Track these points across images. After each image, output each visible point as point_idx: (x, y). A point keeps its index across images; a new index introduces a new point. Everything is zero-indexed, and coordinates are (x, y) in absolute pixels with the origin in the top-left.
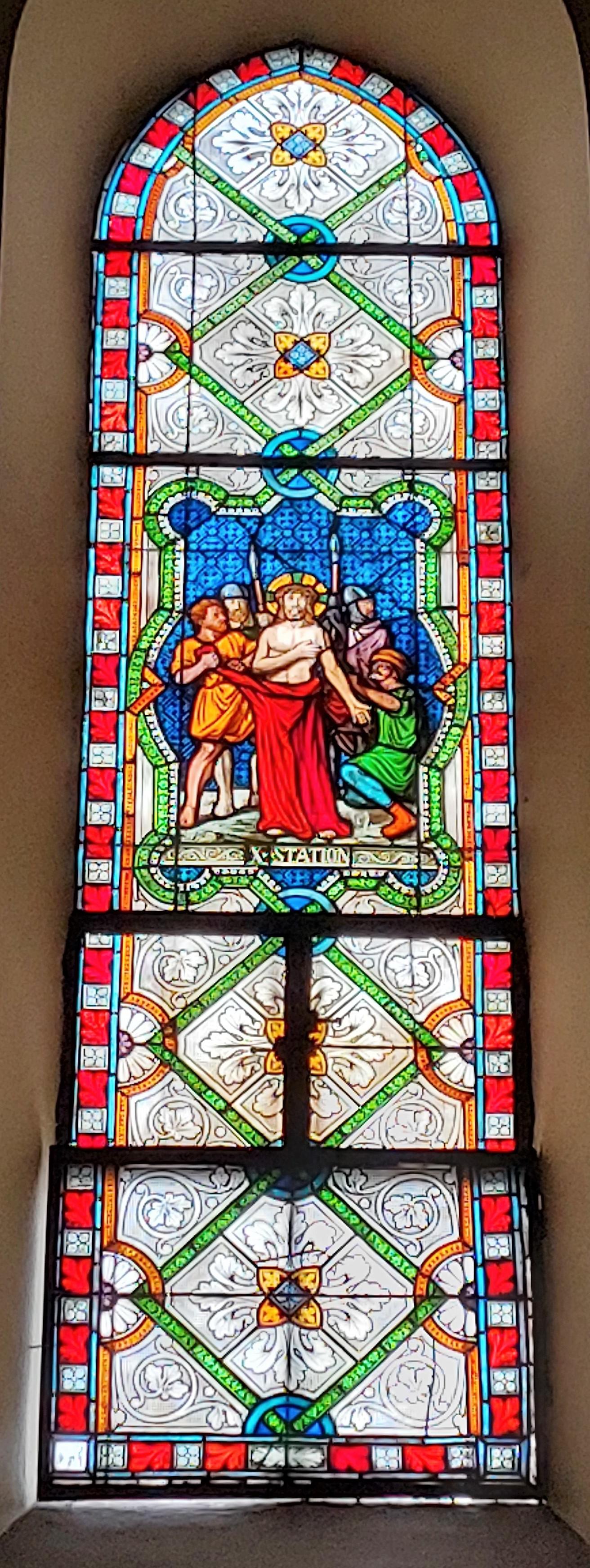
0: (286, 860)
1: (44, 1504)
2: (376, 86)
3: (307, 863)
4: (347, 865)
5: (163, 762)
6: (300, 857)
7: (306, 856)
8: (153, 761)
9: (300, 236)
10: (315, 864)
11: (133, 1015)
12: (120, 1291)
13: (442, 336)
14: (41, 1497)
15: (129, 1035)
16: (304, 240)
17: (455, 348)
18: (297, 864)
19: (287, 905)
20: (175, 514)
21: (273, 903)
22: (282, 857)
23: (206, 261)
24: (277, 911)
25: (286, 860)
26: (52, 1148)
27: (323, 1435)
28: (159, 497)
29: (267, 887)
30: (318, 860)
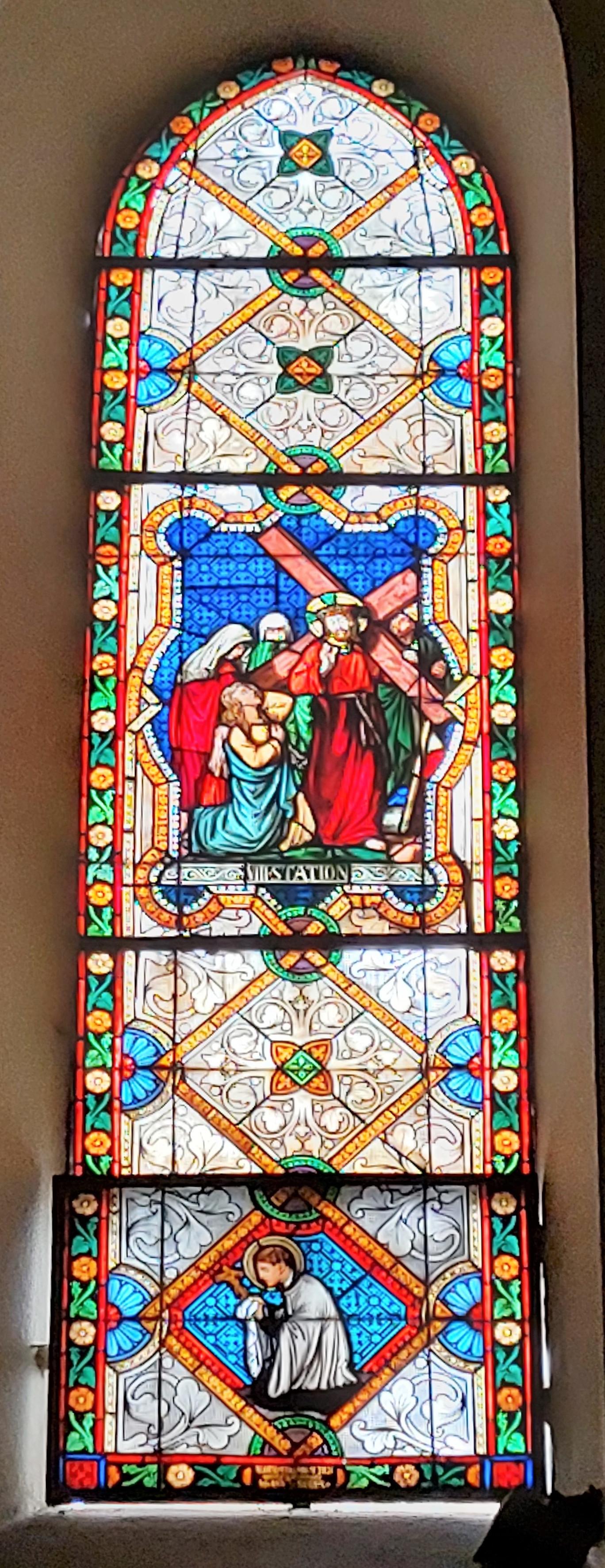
0: (283, 878)
1: (54, 1510)
2: (382, 88)
3: (306, 880)
4: (346, 881)
5: (164, 780)
6: (297, 874)
7: (303, 874)
8: (154, 780)
9: (305, 250)
10: (313, 880)
11: (121, 1286)
12: (140, 1064)
13: (450, 348)
14: (52, 1501)
15: (117, 1307)
16: (311, 253)
17: (462, 359)
18: (295, 881)
19: (289, 927)
20: (428, 538)
21: (275, 926)
22: (279, 876)
23: (207, 277)
24: (279, 933)
25: (283, 878)
26: (55, 1179)
27: (330, 1455)
28: (374, 1384)
29: (269, 908)
30: (317, 877)
